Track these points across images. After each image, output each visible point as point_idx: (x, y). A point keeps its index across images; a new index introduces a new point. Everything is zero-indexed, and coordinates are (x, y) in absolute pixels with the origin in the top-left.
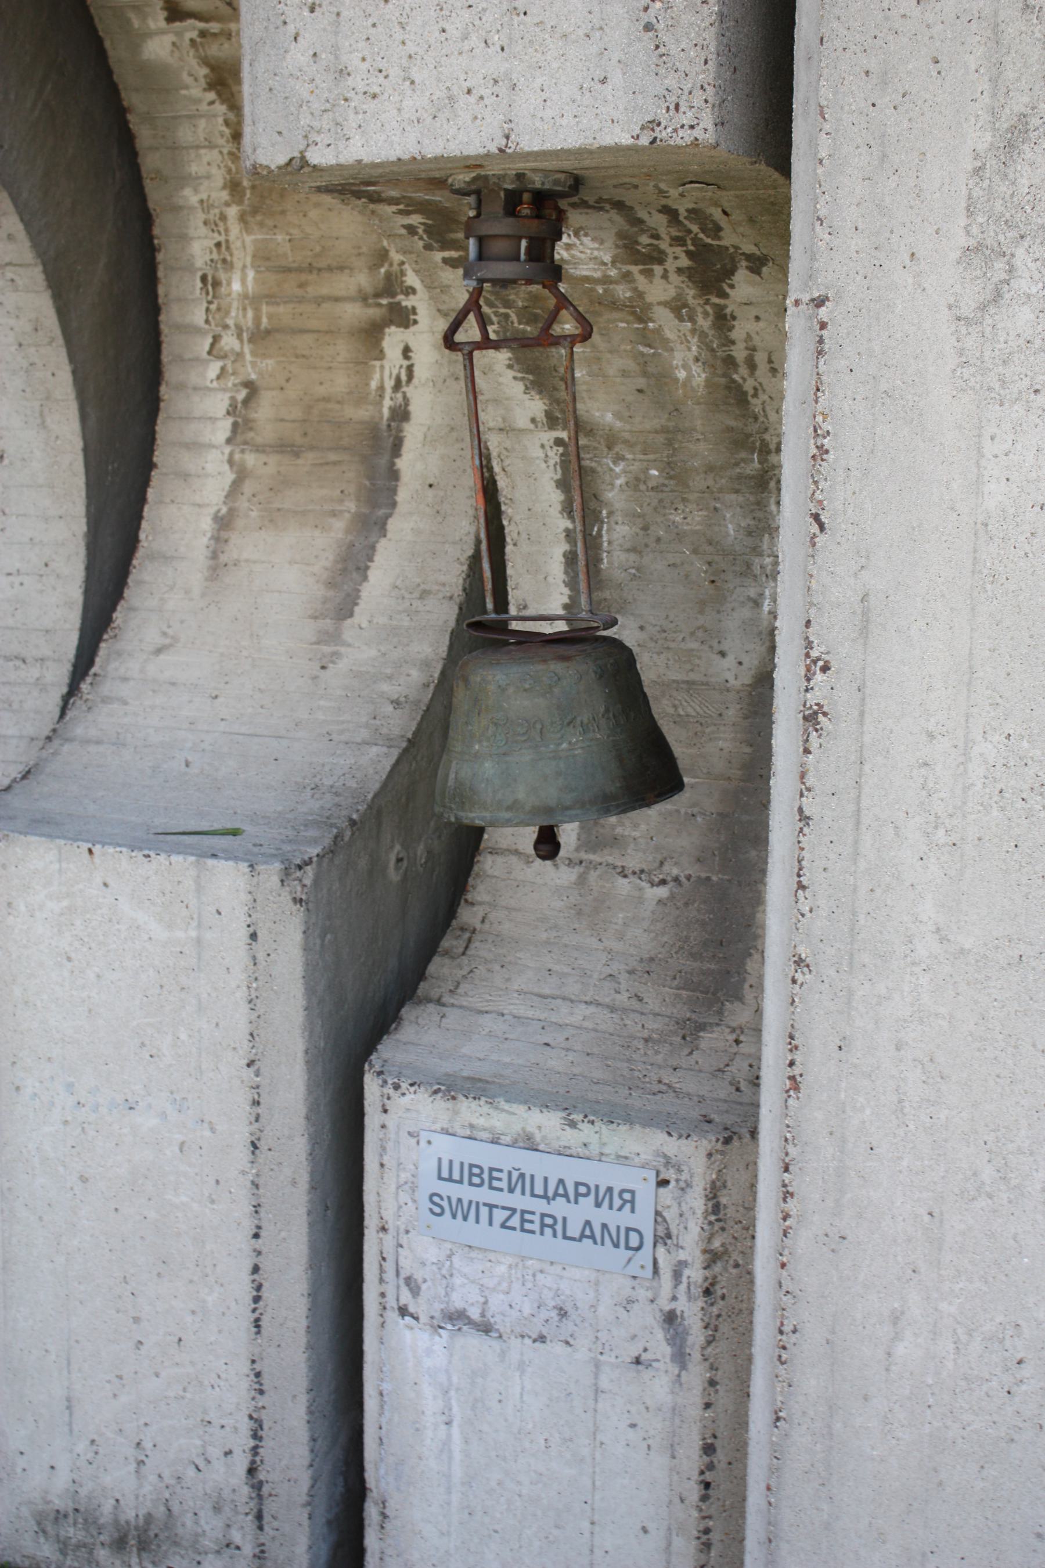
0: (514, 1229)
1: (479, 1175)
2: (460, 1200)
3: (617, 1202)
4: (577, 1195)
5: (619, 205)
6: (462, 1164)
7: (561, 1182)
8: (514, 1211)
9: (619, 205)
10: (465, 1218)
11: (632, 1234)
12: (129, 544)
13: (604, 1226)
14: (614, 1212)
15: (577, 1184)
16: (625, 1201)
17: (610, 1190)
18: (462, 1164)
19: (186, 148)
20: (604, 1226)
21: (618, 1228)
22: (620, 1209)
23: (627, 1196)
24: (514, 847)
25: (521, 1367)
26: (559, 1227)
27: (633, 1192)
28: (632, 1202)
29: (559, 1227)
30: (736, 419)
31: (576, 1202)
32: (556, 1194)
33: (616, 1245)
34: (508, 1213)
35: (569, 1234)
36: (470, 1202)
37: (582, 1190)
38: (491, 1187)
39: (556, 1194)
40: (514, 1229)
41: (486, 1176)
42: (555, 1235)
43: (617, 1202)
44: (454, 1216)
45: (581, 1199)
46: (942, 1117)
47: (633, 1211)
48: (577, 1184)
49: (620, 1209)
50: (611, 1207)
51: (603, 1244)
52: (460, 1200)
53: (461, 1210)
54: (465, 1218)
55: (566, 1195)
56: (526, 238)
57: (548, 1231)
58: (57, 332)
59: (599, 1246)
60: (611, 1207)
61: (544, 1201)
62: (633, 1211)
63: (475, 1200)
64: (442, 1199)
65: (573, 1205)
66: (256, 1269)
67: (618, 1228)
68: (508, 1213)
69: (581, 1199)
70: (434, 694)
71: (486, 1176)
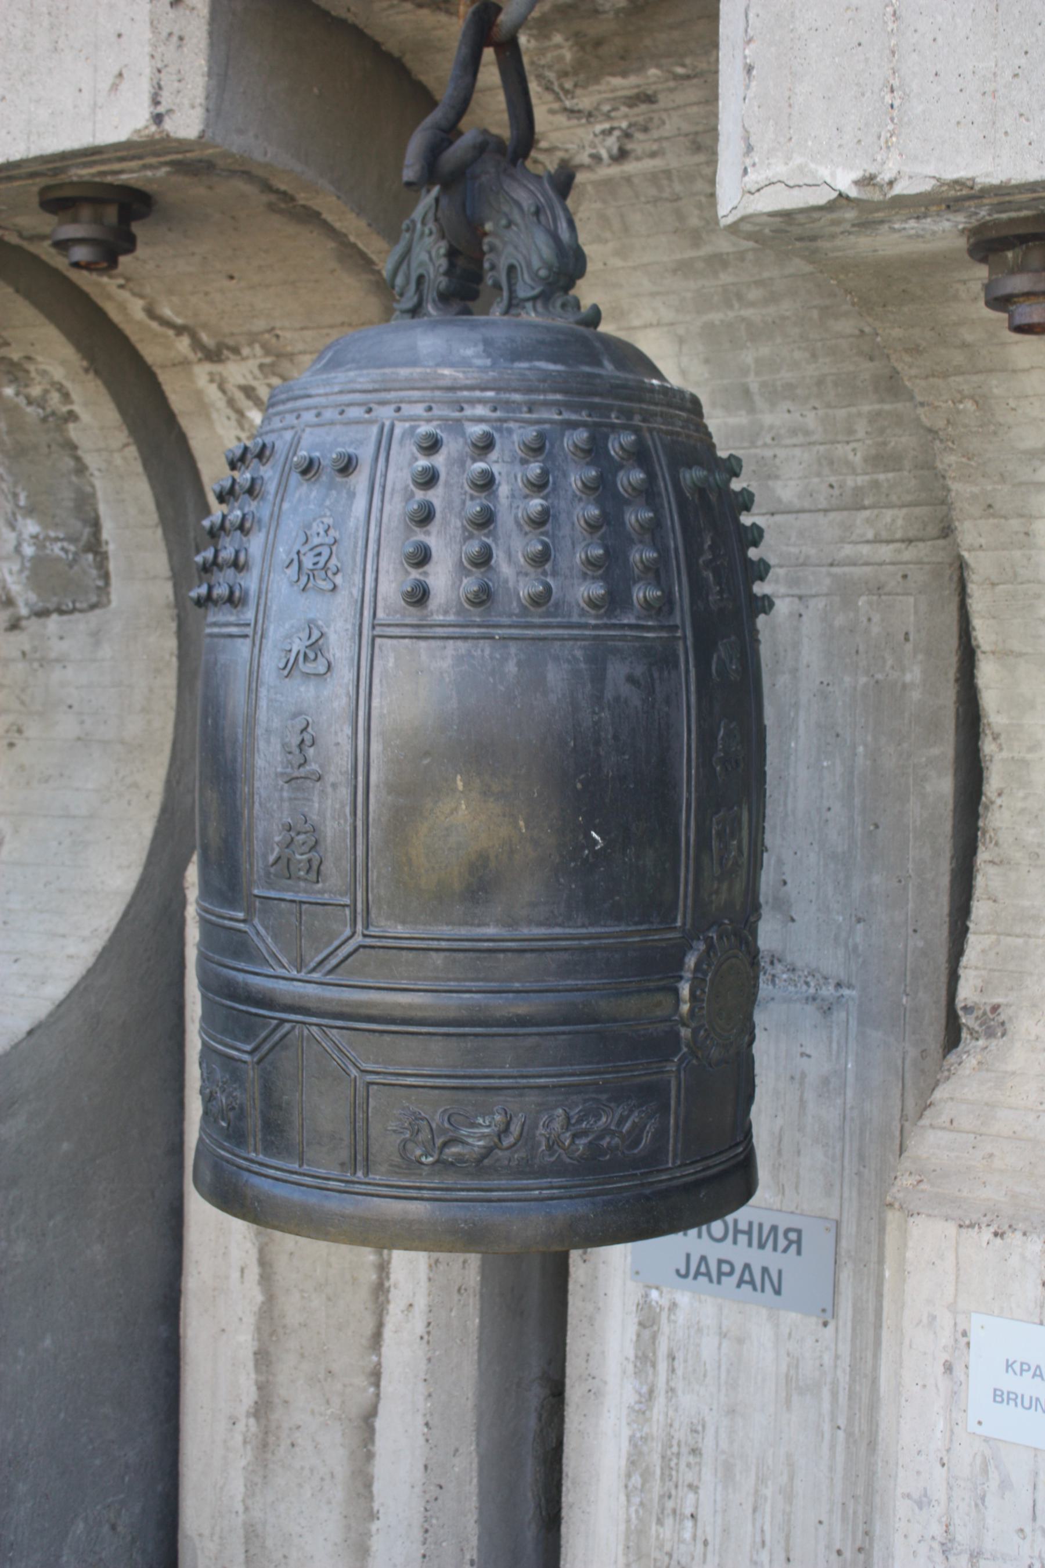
3: (782, 1243)
4: (720, 1274)
5: (780, 181)
6: (1031, 1398)
7: (703, 1259)
9: (780, 181)
13: (765, 1270)
14: (779, 1254)
15: (720, 1262)
16: (791, 1243)
17: (774, 1229)
18: (1031, 1398)
20: (765, 1270)
22: (785, 1250)
23: (793, 1236)
26: (1019, 1400)
27: (799, 1232)
28: (799, 1242)
29: (1019, 1400)
31: (719, 1282)
32: (698, 1273)
37: (726, 1268)
39: (698, 1273)
41: (1005, 1396)
42: (1016, 1405)
43: (782, 1243)
45: (724, 1279)
47: (799, 1252)
48: (720, 1262)
49: (785, 1250)
50: (775, 1249)
51: (763, 1290)
55: (708, 1274)
57: (1012, 1403)
59: (759, 1293)
60: (775, 1249)
62: (799, 1252)
65: (715, 1285)
69: (724, 1279)
71: (1005, 1396)
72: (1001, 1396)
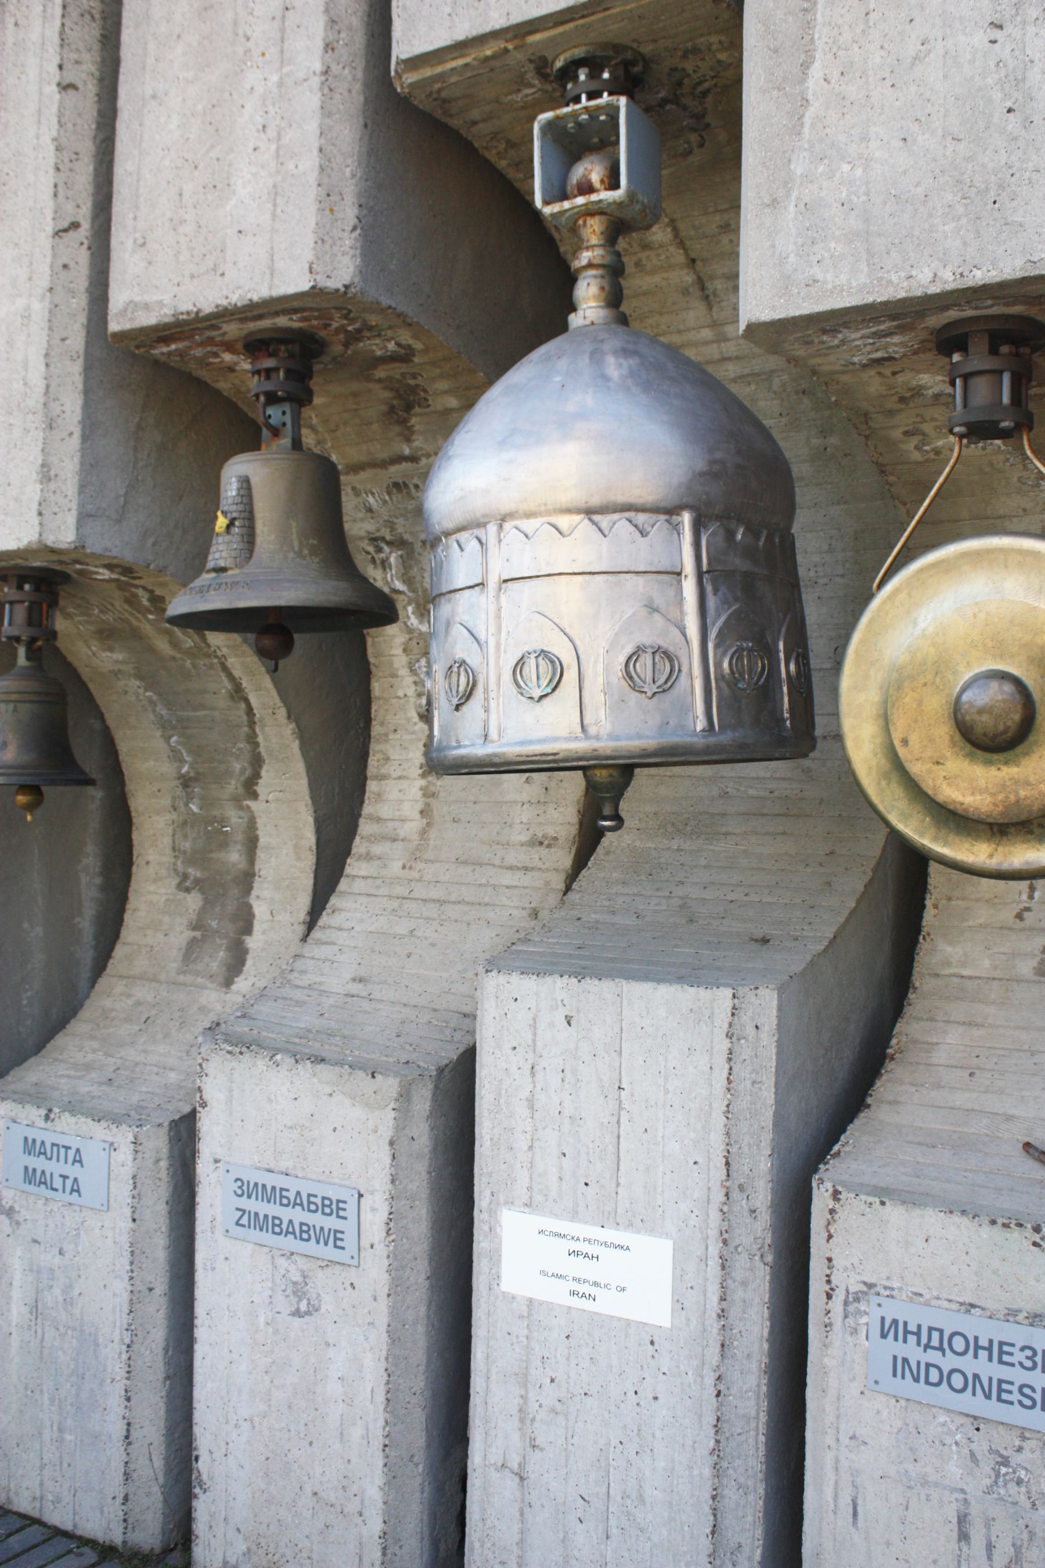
0: (243, 1226)
2: (322, 1229)
8: (244, 1211)
10: (326, 1244)
11: (932, 1370)
12: (351, 830)
21: (990, 1379)
30: (922, 387)
33: (916, 1380)
34: (240, 1213)
36: (330, 1230)
38: (338, 1216)
40: (243, 1226)
41: (334, 1207)
44: (318, 1242)
52: (322, 1229)
53: (260, 1222)
54: (326, 1244)
58: (969, 282)
61: (940, 1353)
64: (1033, 1390)
66: (715, 1526)
68: (240, 1213)
70: (852, 774)
71: (334, 1207)
72: (330, 1206)
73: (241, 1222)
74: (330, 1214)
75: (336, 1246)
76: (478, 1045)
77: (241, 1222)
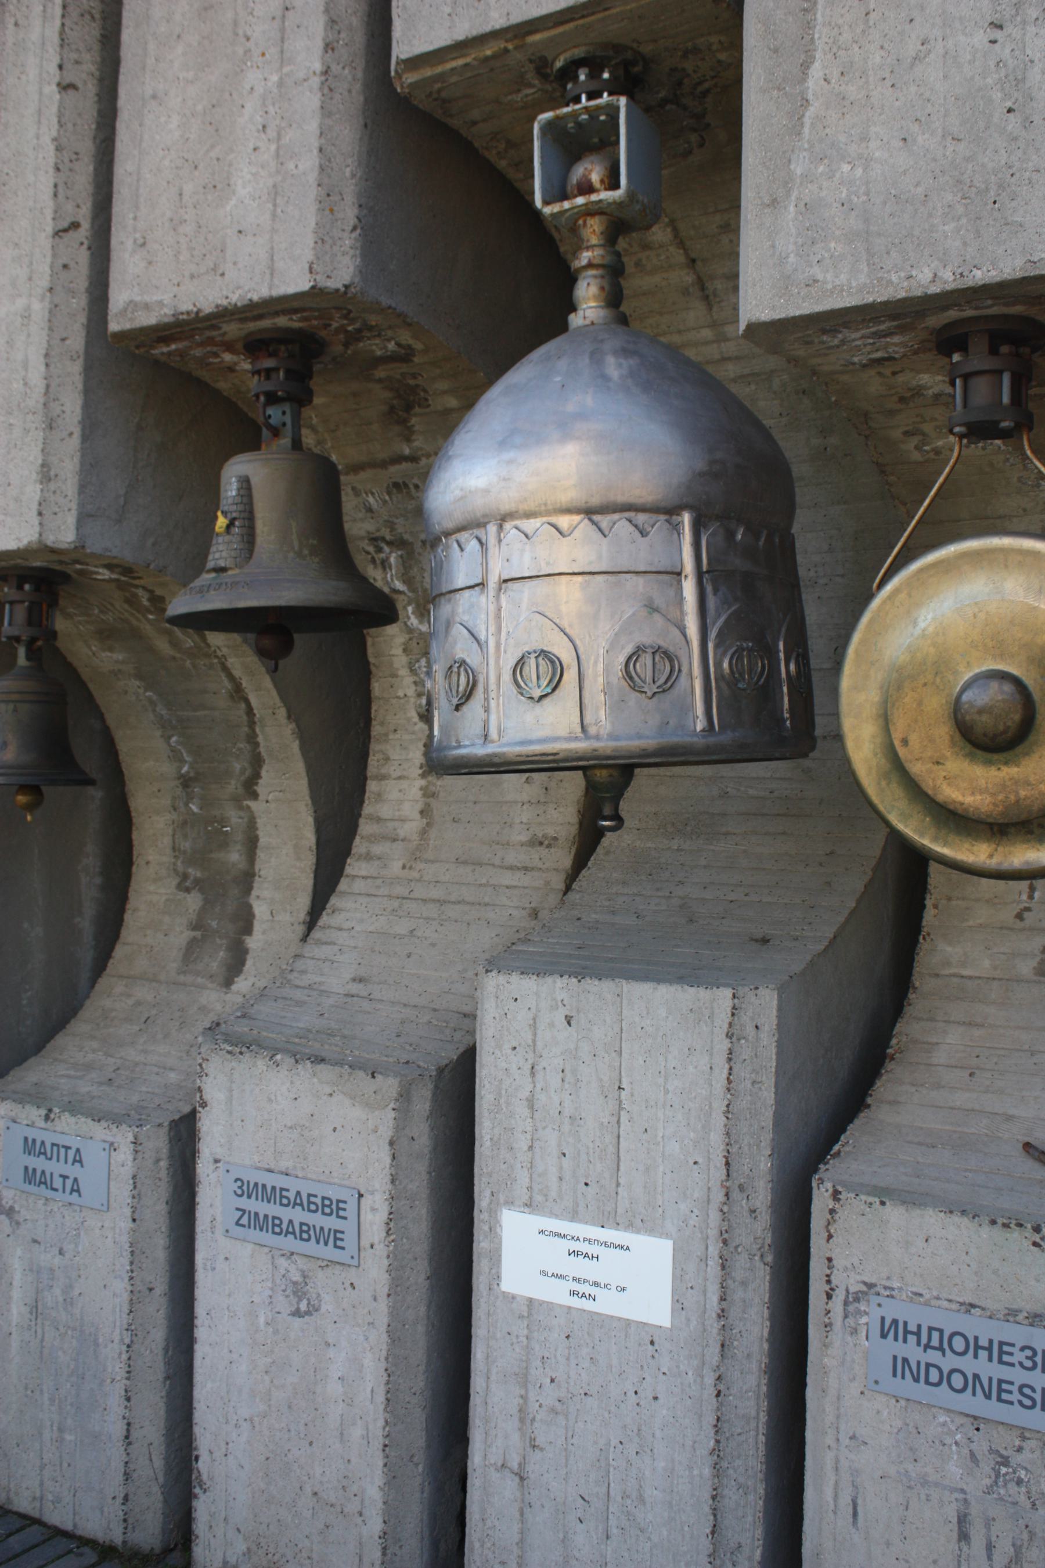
1: (330, 1206)
2: (322, 1229)
8: (244, 1211)
10: (326, 1244)
11: (932, 1370)
19: (448, 534)
21: (990, 1379)
24: (460, 899)
25: (90, 1335)
33: (916, 1380)
34: (240, 1213)
35: (55, 1186)
36: (330, 1230)
38: (338, 1216)
41: (334, 1207)
44: (318, 1242)
46: (411, 755)
52: (322, 1229)
54: (326, 1244)
56: (959, 376)
61: (940, 1353)
63: (333, 1228)
67: (990, 1379)
68: (240, 1213)
71: (334, 1207)
72: (330, 1206)
73: (241, 1222)
74: (331, 1214)
75: (336, 1246)
76: (478, 1045)
77: (241, 1222)
